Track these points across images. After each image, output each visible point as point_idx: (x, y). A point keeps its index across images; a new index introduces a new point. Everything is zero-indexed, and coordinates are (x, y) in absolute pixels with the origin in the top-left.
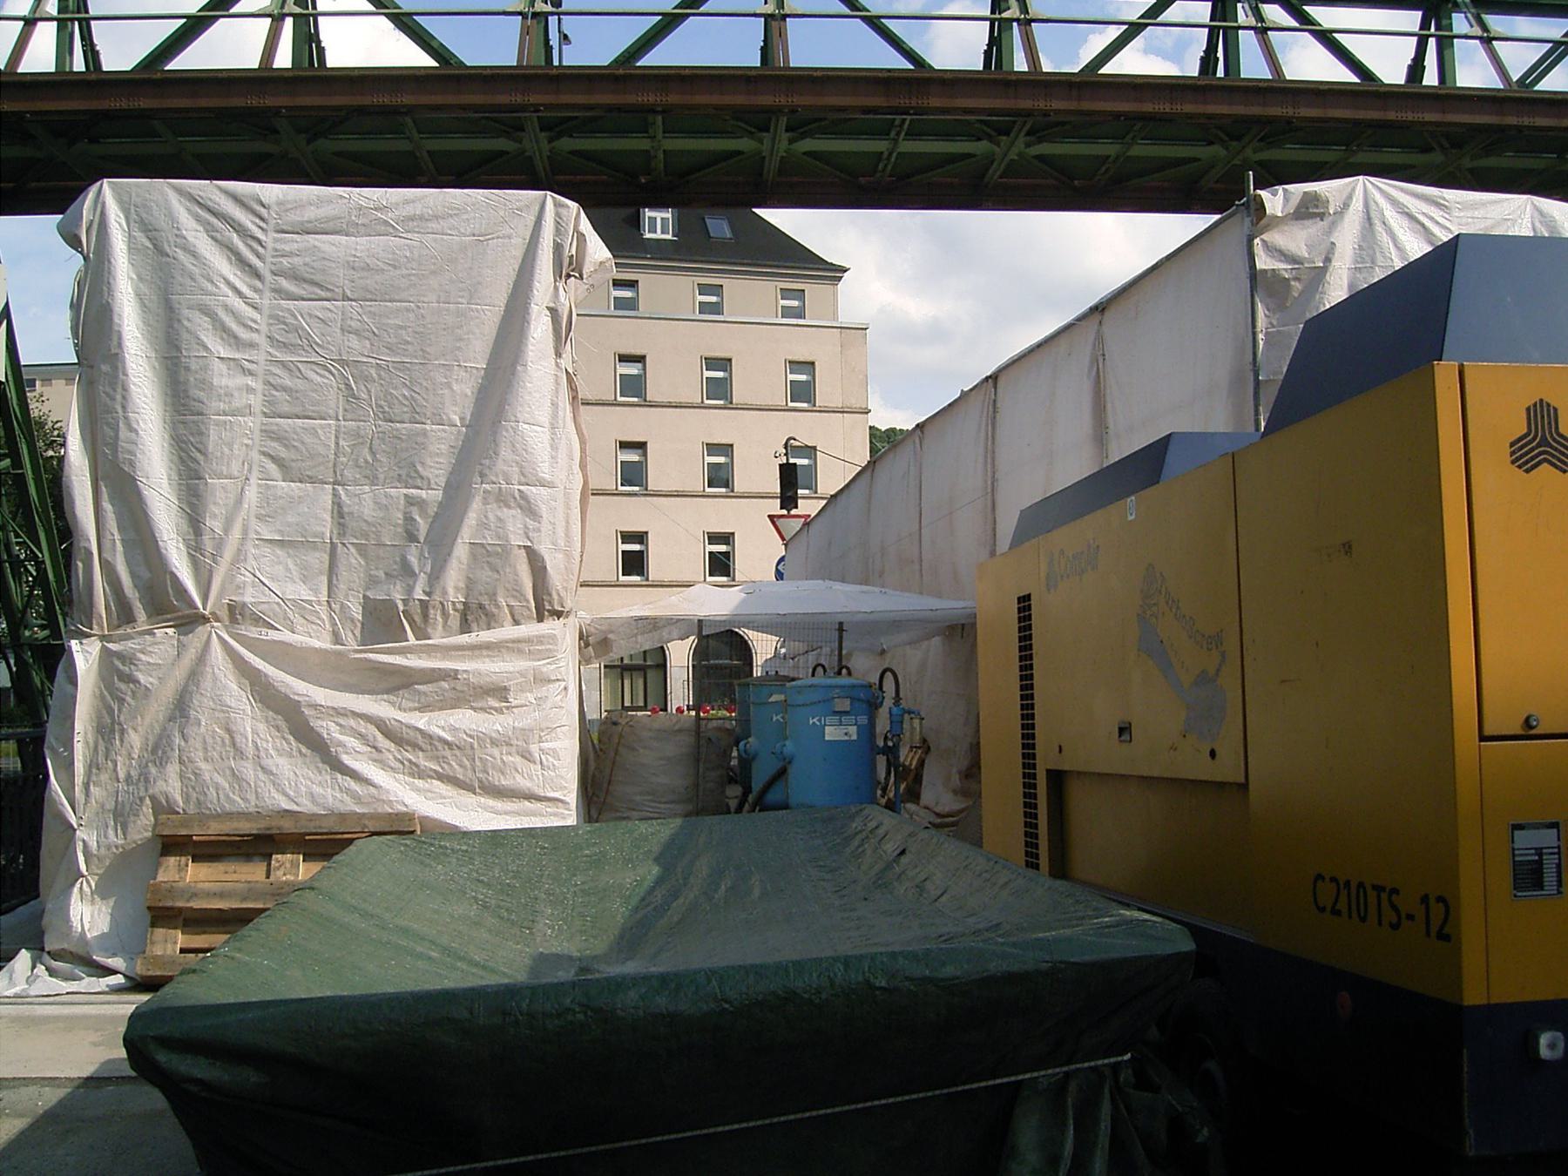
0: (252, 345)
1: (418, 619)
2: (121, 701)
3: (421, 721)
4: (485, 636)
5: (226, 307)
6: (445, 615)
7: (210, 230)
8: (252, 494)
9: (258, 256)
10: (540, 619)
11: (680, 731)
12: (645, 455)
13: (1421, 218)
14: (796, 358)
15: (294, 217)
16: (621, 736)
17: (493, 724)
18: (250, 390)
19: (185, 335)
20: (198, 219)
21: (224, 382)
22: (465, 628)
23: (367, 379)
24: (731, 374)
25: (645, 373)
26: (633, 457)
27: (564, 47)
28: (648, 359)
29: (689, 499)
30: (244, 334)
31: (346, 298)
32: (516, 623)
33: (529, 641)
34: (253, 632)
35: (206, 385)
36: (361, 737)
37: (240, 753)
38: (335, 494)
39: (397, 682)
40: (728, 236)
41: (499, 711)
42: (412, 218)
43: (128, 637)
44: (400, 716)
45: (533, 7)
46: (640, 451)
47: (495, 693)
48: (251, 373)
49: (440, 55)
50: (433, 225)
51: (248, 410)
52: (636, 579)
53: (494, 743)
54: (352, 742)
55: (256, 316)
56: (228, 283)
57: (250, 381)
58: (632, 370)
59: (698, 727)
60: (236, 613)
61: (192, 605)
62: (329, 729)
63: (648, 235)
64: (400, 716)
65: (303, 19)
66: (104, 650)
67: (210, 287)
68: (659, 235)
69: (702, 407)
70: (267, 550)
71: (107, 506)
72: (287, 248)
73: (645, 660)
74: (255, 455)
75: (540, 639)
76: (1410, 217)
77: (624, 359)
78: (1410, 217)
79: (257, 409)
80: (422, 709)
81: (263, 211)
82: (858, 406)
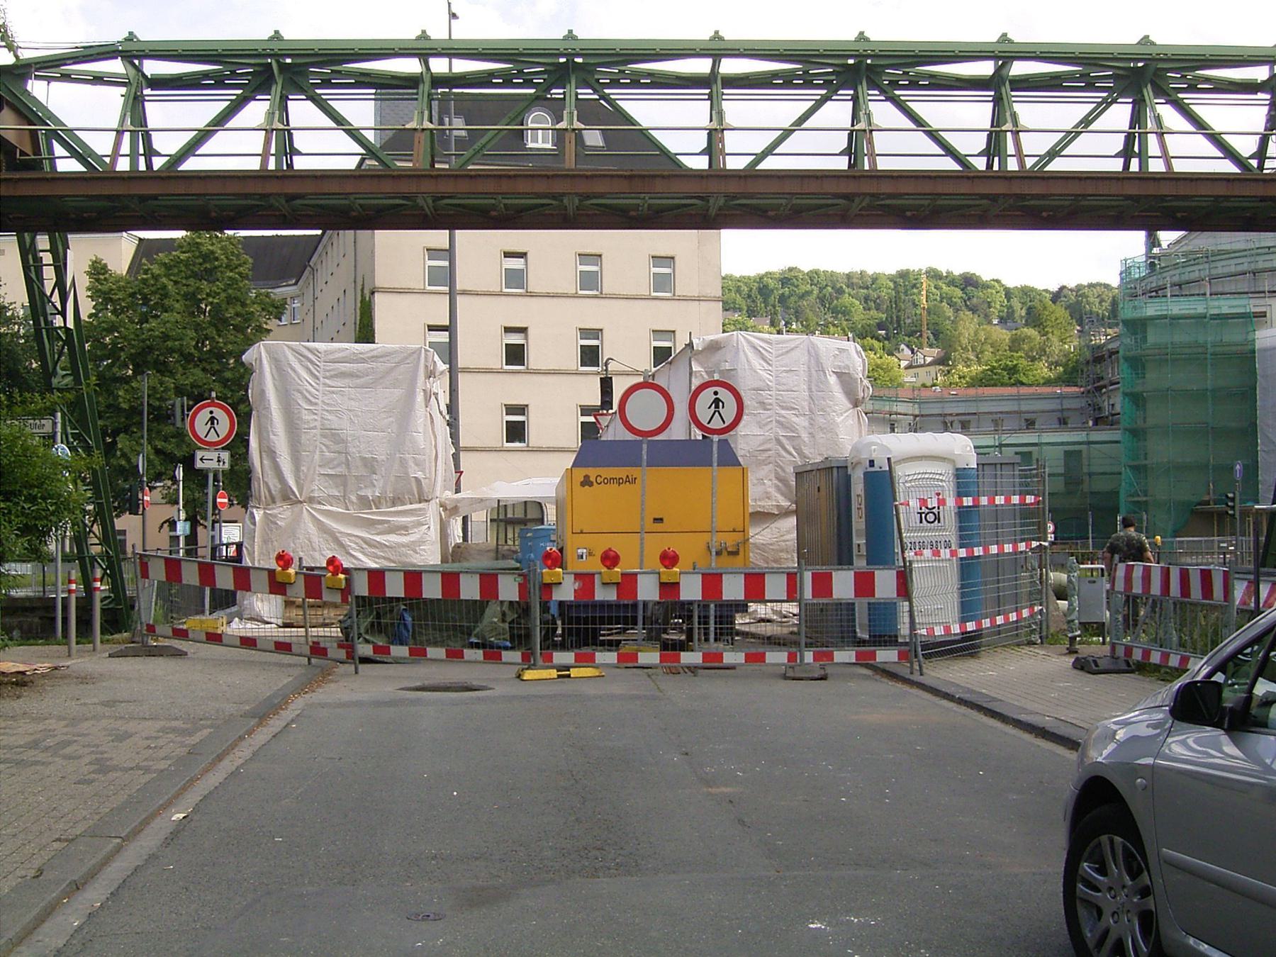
0: (316, 404)
1: (377, 502)
2: (272, 530)
3: (378, 538)
4: (400, 508)
5: (306, 390)
6: (386, 502)
7: (300, 361)
8: (317, 457)
9: (318, 371)
10: (420, 503)
11: (489, 551)
12: (526, 338)
13: (761, 349)
14: (658, 254)
15: (331, 357)
16: (461, 553)
17: (404, 540)
18: (316, 420)
19: (292, 402)
20: (296, 357)
21: (307, 417)
22: (394, 505)
23: (357, 416)
24: (601, 267)
25: (527, 268)
26: (516, 339)
27: (452, 21)
28: (528, 255)
29: (477, 454)
30: (313, 400)
31: (350, 387)
32: (411, 504)
33: (415, 510)
34: (318, 507)
35: (300, 418)
36: (356, 543)
37: (314, 550)
38: (346, 457)
39: (370, 524)
40: (601, 145)
41: (405, 535)
42: (373, 357)
43: (274, 509)
44: (370, 536)
45: (422, 125)
46: (523, 335)
47: (403, 529)
48: (316, 414)
49: (367, 147)
50: (381, 360)
51: (315, 428)
52: (517, 445)
53: (403, 546)
54: (353, 545)
55: (317, 393)
56: (307, 381)
57: (315, 417)
58: (516, 264)
59: (497, 548)
60: (311, 500)
61: (296, 497)
62: (346, 541)
63: (530, 145)
64: (370, 536)
65: (282, 132)
66: (265, 512)
67: (299, 382)
68: (540, 145)
69: (575, 296)
70: (322, 477)
71: (265, 462)
72: (328, 368)
73: (526, 516)
74: (318, 443)
75: (420, 509)
76: (755, 348)
77: (508, 255)
78: (755, 348)
79: (319, 427)
80: (378, 534)
81: (319, 355)
82: (712, 295)
